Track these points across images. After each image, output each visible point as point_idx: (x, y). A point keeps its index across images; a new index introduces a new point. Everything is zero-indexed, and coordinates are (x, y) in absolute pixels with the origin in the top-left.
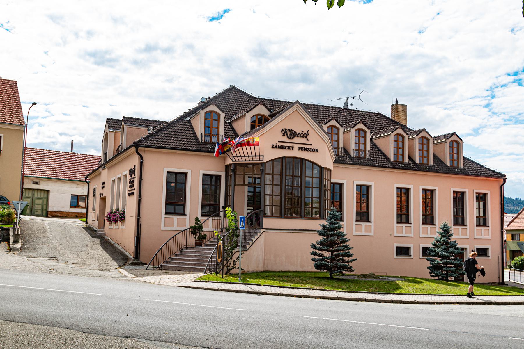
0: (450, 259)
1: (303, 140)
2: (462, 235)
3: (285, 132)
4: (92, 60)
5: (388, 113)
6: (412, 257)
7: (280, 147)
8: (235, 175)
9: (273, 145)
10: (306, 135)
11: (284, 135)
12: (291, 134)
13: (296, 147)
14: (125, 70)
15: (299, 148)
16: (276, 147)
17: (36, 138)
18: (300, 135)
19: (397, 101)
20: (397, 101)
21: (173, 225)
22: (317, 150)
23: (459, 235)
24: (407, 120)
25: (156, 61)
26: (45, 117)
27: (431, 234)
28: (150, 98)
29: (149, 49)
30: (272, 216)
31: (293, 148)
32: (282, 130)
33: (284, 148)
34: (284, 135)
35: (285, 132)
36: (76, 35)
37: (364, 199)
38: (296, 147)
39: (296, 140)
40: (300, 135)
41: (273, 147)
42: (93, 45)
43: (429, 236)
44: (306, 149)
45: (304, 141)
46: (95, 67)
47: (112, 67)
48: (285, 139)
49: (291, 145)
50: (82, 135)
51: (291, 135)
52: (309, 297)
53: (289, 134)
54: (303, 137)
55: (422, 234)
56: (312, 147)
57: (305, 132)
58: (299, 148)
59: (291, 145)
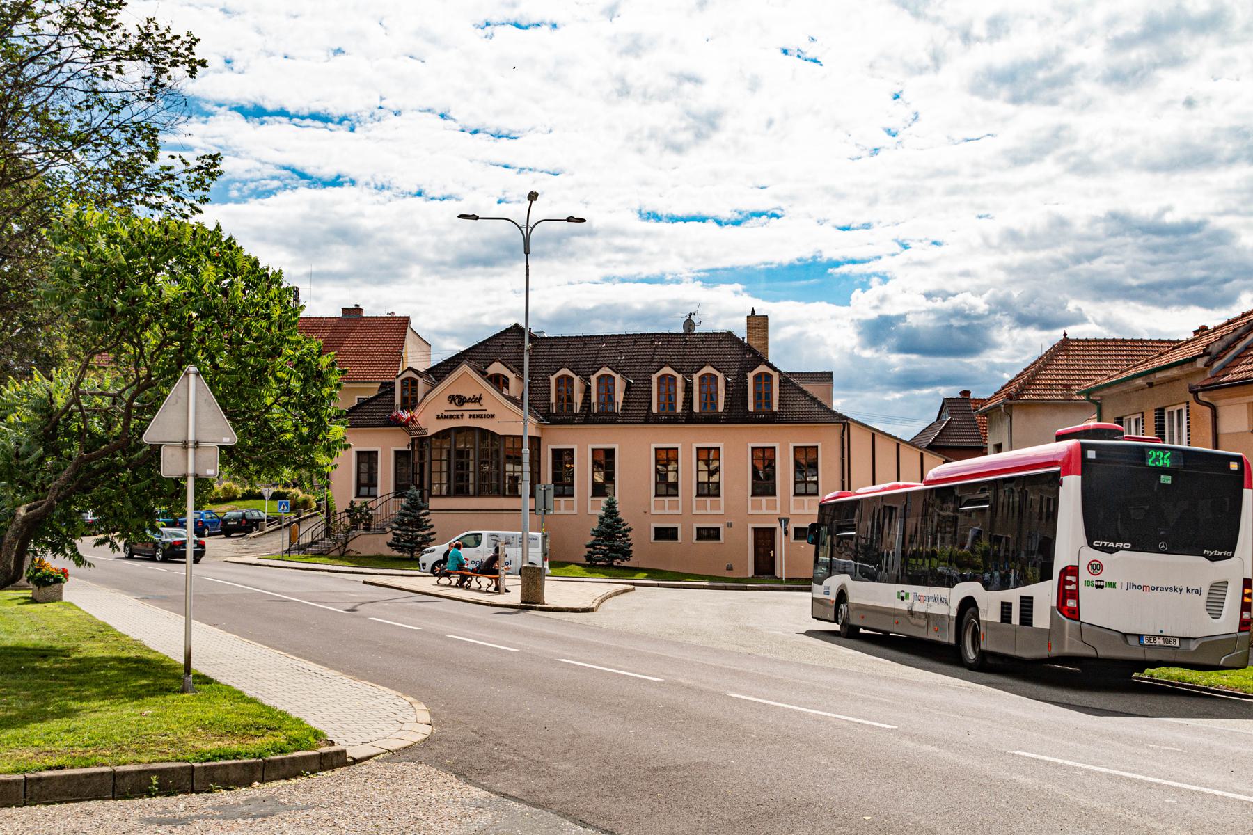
0: (999, 551)
1: (476, 406)
2: (767, 508)
3: (452, 399)
4: (1005, 92)
5: (741, 333)
6: (722, 540)
7: (446, 417)
8: (431, 449)
9: (438, 416)
10: (478, 400)
11: (451, 402)
12: (460, 400)
13: (467, 414)
14: (1087, 105)
15: (470, 416)
16: (442, 417)
17: (876, 307)
18: (470, 401)
19: (753, 312)
20: (753, 312)
21: (664, 508)
22: (493, 416)
23: (804, 509)
24: (767, 338)
25: (1176, 61)
26: (893, 255)
27: (767, 509)
28: (1154, 167)
29: (1155, 30)
30: (440, 496)
31: (462, 416)
32: (449, 397)
33: (451, 417)
34: (451, 402)
35: (452, 399)
36: (967, 37)
37: (536, 469)
38: (467, 414)
39: (467, 406)
40: (470, 401)
41: (438, 417)
42: (1001, 54)
43: (807, 512)
44: (478, 416)
45: (476, 406)
46: (1010, 109)
47: (1053, 102)
48: (453, 407)
49: (460, 413)
50: (979, 292)
51: (459, 402)
52: (286, 568)
53: (457, 401)
54: (475, 402)
55: (697, 509)
56: (486, 413)
57: (478, 396)
58: (470, 416)
59: (460, 413)
